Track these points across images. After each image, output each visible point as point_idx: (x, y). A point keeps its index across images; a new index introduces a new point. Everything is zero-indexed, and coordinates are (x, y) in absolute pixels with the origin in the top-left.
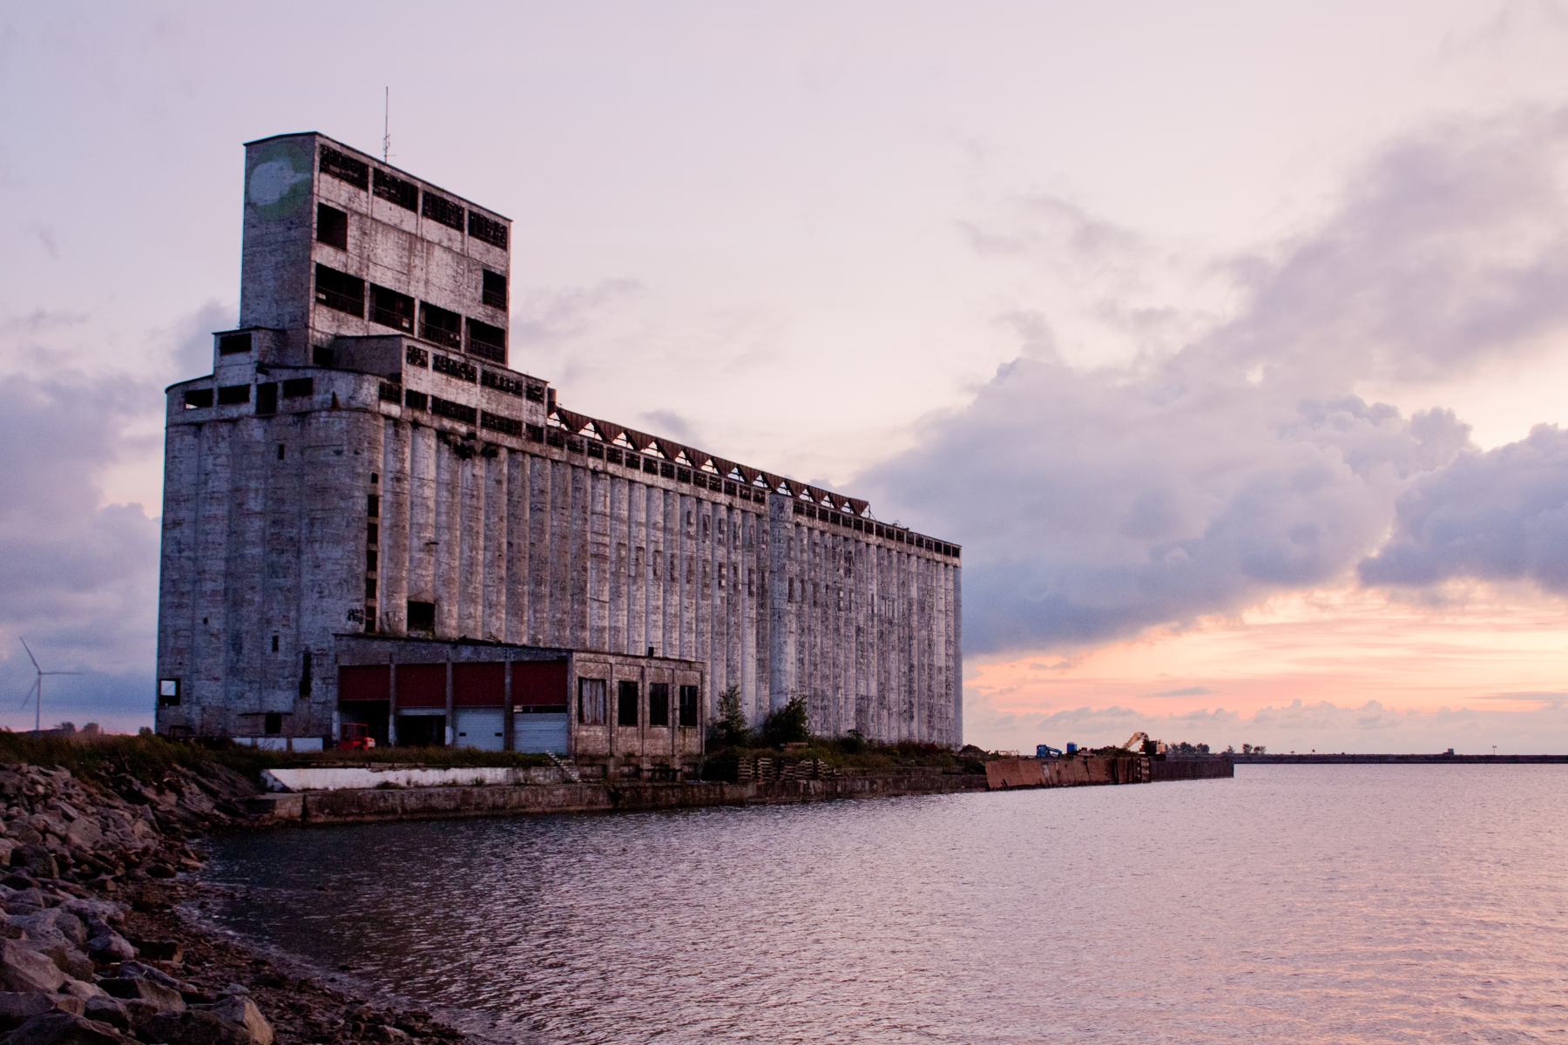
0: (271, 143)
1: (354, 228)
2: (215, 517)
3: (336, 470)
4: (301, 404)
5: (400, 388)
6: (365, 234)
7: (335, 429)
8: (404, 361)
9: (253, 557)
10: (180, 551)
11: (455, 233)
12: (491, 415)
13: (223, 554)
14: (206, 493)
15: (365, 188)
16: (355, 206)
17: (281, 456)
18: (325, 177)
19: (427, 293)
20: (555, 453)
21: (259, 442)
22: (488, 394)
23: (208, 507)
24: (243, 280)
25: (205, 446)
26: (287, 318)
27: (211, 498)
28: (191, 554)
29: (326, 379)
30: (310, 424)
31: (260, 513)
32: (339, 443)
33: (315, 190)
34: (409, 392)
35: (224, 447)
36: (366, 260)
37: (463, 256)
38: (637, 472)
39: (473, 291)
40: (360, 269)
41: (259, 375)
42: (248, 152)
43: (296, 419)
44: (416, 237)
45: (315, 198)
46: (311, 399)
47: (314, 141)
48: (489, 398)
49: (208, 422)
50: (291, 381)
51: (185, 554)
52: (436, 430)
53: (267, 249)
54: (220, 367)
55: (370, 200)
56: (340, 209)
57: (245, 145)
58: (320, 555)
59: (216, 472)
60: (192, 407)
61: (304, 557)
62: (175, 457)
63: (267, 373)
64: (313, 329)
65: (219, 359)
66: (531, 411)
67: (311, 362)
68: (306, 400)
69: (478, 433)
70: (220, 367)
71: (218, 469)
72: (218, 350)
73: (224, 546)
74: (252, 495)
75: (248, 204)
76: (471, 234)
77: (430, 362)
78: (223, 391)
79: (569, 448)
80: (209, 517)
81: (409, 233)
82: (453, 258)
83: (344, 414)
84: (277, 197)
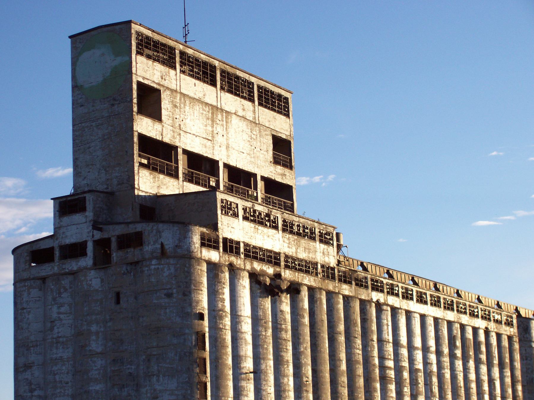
0: (92, 33)
1: (167, 102)
2: (61, 358)
3: (168, 311)
4: (133, 254)
5: (218, 236)
6: (176, 106)
7: (165, 275)
8: (219, 212)
9: (97, 392)
10: (31, 391)
11: (248, 104)
12: (292, 258)
13: (70, 392)
14: (53, 338)
15: (174, 68)
16: (166, 83)
17: (118, 302)
18: (140, 59)
19: (228, 156)
20: (345, 289)
21: (97, 291)
22: (289, 239)
23: (55, 351)
24: (74, 152)
25: (50, 298)
26: (115, 182)
27: (57, 343)
28: (41, 393)
29: (155, 231)
30: (142, 272)
31: (101, 353)
32: (169, 286)
33: (134, 70)
34: (225, 240)
35: (66, 297)
36: (179, 129)
37: (255, 123)
38: (411, 302)
39: (265, 153)
40: (174, 137)
41: (95, 232)
42: (73, 43)
43: (129, 268)
44: (217, 108)
45: (134, 77)
46: (141, 250)
47: (130, 28)
48: (289, 243)
49: (51, 275)
50: (123, 235)
51: (36, 393)
52: (248, 271)
53: (94, 124)
54: (59, 228)
55: (178, 78)
56: (155, 86)
57: (70, 37)
58: (158, 388)
59: (61, 320)
60: (34, 265)
61: (143, 390)
62: (23, 309)
63: (100, 230)
64: (139, 189)
65: (58, 221)
66: (323, 253)
67: (138, 219)
68: (137, 251)
69: (283, 274)
70: (59, 228)
71: (62, 316)
72: (57, 213)
73: (70, 384)
74: (94, 337)
75: (75, 87)
76: (260, 104)
77: (241, 213)
78: (62, 248)
79: (357, 285)
80: (56, 359)
81: (211, 105)
82: (247, 125)
83: (172, 261)
84: (100, 79)
